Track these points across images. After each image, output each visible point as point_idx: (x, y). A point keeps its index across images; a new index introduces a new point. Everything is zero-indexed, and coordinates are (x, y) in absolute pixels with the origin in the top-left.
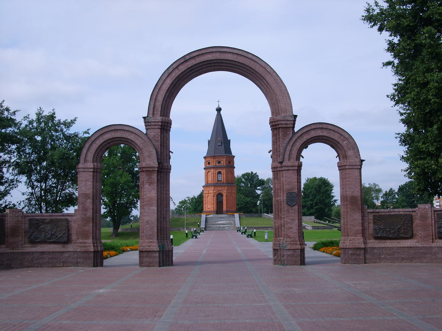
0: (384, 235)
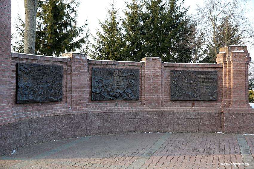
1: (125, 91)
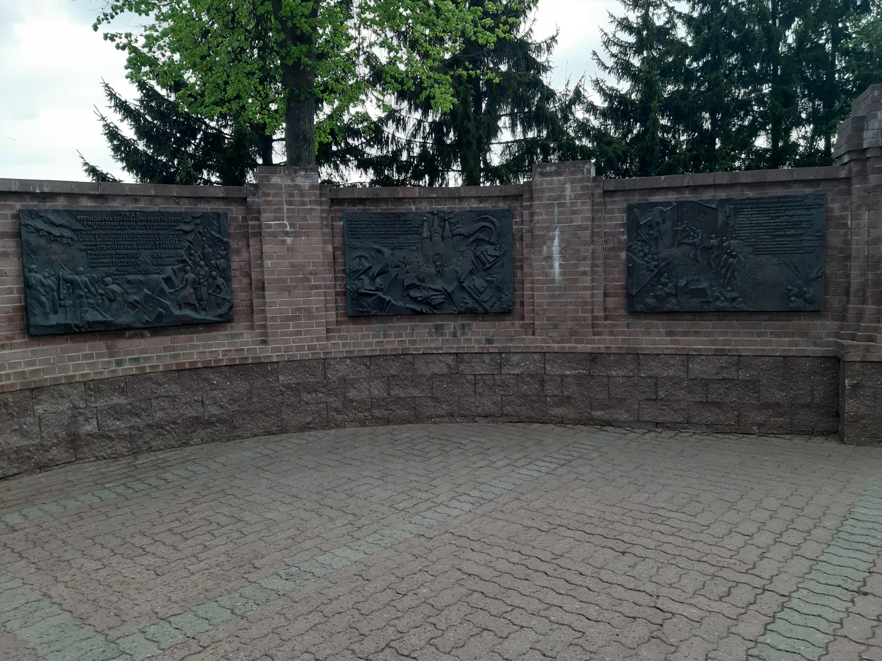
0: (92, 316)
1: (464, 284)
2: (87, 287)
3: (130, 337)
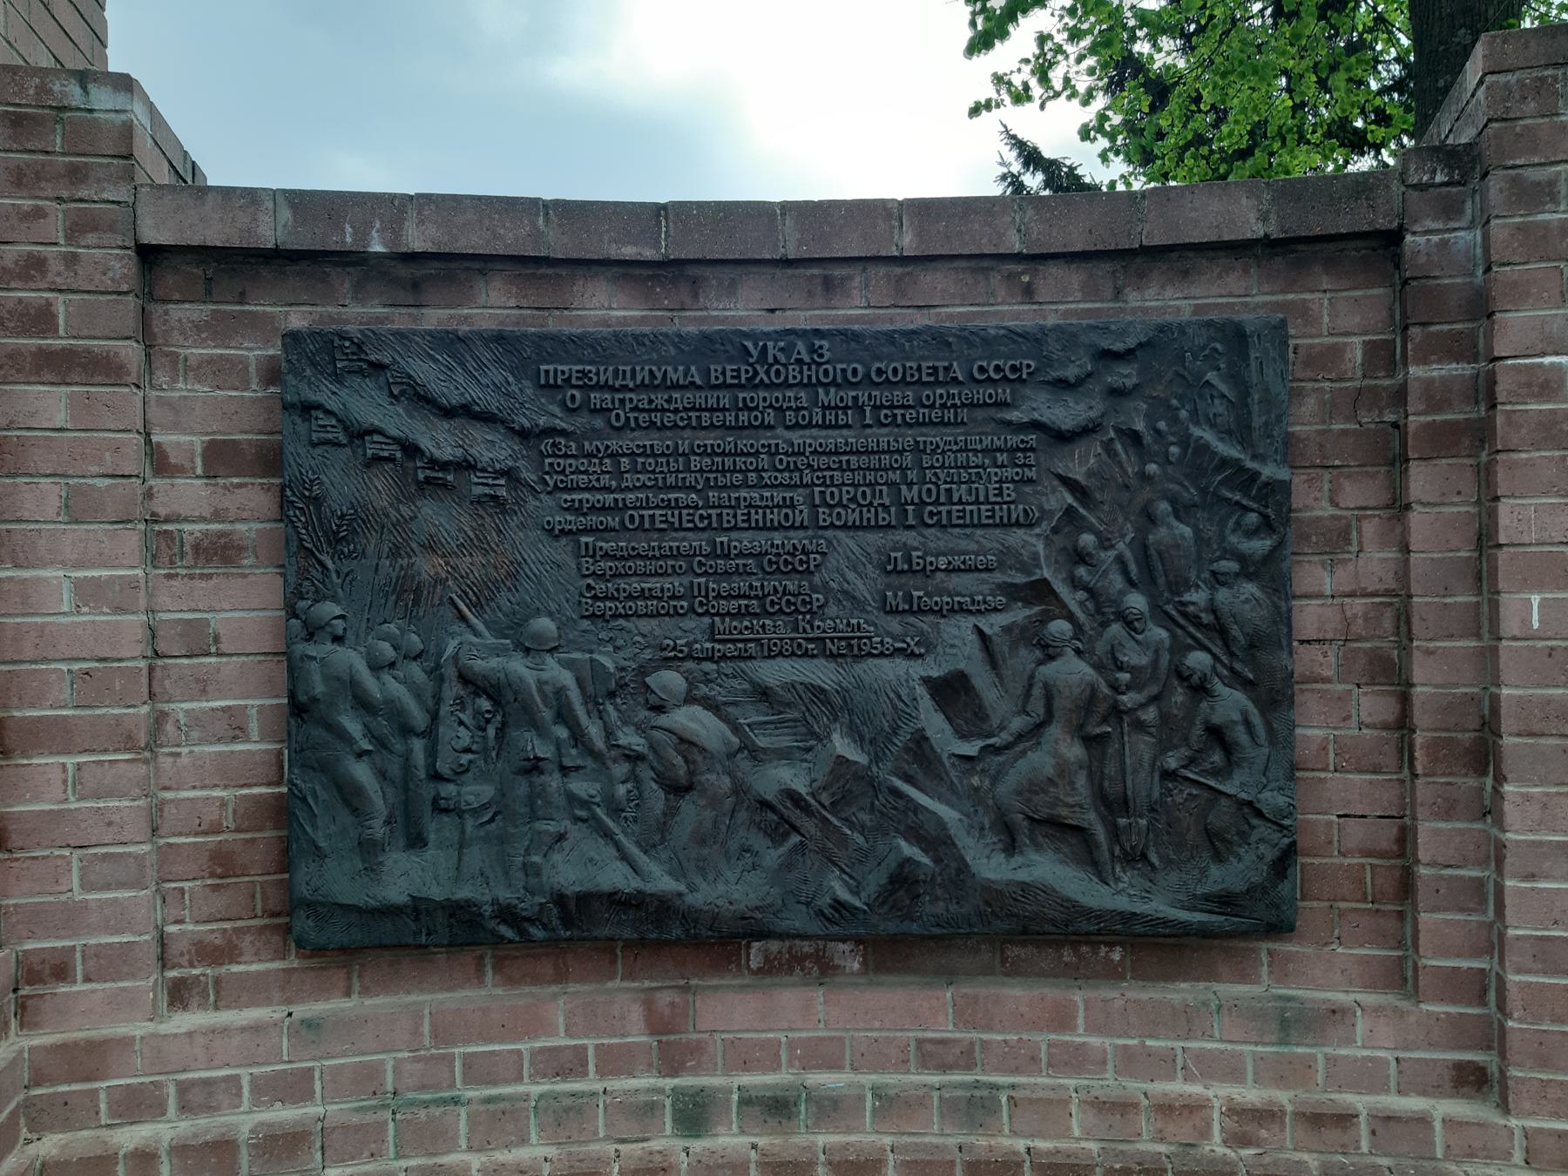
0: (585, 866)
2: (564, 715)
3: (770, 968)
